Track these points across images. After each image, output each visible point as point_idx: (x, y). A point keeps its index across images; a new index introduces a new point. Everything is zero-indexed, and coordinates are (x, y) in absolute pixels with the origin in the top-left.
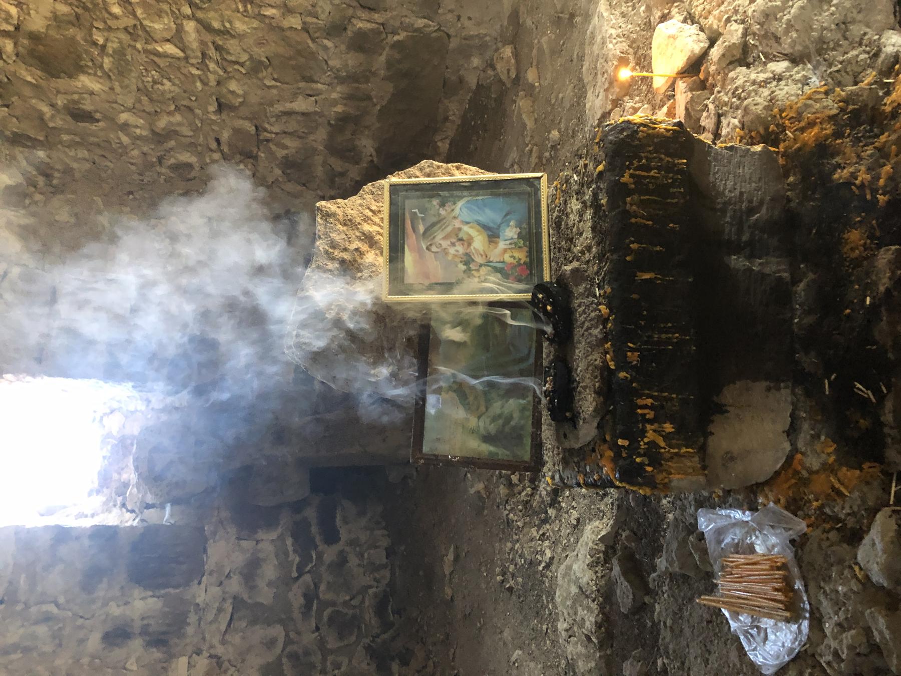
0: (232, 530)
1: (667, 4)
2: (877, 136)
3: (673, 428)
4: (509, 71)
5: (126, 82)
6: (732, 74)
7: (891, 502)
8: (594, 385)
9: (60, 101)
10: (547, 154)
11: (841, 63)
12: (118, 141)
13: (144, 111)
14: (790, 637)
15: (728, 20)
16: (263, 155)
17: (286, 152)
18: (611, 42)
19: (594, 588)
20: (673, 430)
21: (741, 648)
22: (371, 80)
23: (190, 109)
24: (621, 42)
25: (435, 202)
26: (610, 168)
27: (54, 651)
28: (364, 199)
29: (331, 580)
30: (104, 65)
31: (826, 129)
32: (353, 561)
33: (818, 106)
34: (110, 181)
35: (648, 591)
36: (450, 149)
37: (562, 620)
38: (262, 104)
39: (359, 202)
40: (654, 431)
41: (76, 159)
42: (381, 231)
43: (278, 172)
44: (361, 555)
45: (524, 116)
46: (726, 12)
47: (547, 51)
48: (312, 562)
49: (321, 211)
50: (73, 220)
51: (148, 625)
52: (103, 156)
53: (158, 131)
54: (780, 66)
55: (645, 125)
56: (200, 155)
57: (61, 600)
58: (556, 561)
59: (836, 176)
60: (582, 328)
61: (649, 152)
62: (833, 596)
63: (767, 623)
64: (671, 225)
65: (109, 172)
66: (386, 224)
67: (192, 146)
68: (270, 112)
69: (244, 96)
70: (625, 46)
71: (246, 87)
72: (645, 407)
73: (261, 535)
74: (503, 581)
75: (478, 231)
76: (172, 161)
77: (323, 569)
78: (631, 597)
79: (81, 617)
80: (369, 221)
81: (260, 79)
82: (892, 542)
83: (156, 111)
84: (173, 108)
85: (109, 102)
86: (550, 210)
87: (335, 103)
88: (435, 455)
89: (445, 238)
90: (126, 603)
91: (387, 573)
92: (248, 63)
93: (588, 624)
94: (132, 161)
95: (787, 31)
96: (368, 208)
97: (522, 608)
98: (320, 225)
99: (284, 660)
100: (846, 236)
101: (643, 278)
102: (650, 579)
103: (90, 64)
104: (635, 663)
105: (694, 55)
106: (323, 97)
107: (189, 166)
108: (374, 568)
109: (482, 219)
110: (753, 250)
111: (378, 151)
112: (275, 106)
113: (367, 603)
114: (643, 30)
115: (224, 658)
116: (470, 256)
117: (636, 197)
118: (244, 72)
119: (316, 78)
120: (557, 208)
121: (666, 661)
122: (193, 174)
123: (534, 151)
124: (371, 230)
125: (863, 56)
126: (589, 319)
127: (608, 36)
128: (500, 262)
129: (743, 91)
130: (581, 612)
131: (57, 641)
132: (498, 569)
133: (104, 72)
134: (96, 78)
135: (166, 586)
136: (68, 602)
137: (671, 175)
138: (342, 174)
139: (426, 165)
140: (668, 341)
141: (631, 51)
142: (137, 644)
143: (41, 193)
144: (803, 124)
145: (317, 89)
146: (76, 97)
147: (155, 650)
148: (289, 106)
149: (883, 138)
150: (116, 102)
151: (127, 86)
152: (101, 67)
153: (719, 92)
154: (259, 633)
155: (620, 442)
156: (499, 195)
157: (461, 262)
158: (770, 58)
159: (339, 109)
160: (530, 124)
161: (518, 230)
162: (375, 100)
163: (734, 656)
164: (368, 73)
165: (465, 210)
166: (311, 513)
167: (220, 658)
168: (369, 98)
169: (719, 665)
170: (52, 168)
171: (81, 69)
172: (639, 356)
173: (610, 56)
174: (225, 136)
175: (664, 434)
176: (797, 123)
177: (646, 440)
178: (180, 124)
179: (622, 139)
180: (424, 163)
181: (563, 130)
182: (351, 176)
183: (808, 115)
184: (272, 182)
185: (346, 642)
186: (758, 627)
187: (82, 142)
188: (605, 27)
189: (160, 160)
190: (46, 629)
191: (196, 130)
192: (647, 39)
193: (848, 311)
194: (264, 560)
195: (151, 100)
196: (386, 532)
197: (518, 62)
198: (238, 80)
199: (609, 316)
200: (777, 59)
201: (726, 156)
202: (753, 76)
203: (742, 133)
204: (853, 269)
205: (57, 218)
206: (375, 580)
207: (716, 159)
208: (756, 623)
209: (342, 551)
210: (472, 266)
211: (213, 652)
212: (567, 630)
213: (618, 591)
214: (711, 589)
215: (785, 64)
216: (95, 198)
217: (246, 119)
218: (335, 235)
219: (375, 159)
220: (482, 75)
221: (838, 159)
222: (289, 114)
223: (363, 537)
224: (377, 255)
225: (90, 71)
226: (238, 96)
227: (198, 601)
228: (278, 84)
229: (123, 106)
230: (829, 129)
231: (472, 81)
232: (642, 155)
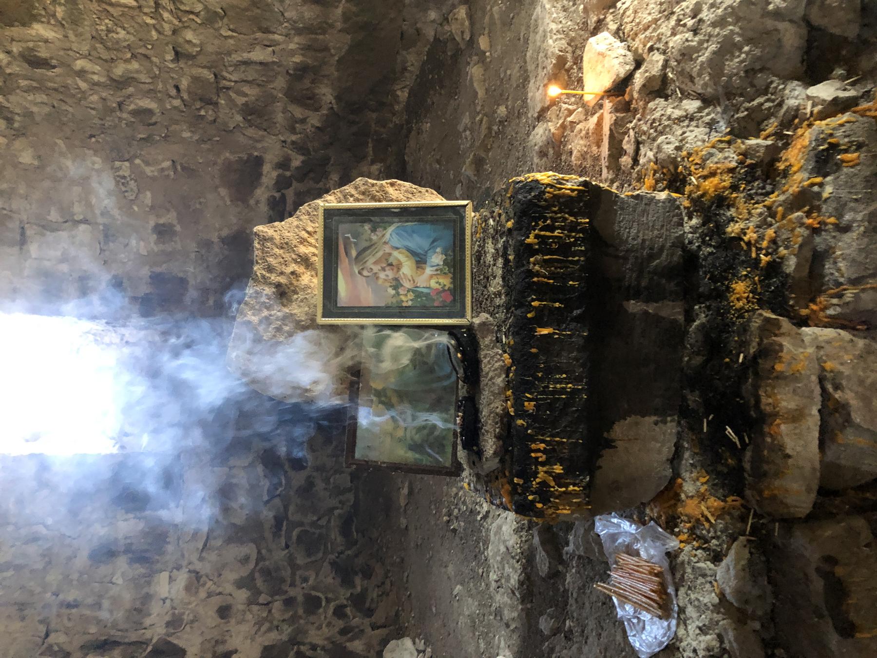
1: (603, 9)
2: (767, 194)
3: (562, 469)
4: (463, 32)
5: (80, 30)
6: (651, 105)
7: (747, 533)
8: (495, 431)
9: (15, 48)
10: (495, 128)
11: (747, 109)
12: (76, 87)
13: (100, 58)
14: (662, 631)
15: (651, 49)
16: (223, 102)
18: (551, 38)
19: (519, 551)
20: (562, 471)
21: (624, 631)
22: (329, 31)
23: (146, 57)
24: (561, 39)
25: (367, 227)
26: (518, 227)
28: (301, 220)
30: (57, 14)
31: (725, 181)
32: (320, 485)
33: (720, 155)
34: (71, 124)
35: (561, 561)
36: (409, 96)
37: (493, 571)
38: (221, 53)
39: (296, 223)
40: (546, 472)
42: (316, 252)
43: (239, 118)
45: (475, 85)
46: (650, 38)
47: (498, 22)
49: (259, 236)
50: (36, 163)
51: (131, 544)
53: (114, 77)
54: (692, 105)
55: (552, 186)
56: (160, 101)
58: (491, 515)
59: (729, 229)
60: (487, 377)
61: (555, 212)
62: (696, 603)
63: (646, 616)
64: (571, 283)
65: (70, 116)
66: (320, 245)
67: (151, 93)
68: (228, 61)
69: (201, 45)
70: (563, 43)
71: (201, 37)
72: (539, 450)
74: (448, 521)
75: (407, 257)
78: (547, 565)
80: (305, 243)
81: (215, 29)
82: (744, 570)
83: (112, 59)
84: (129, 55)
85: (65, 49)
86: (473, 243)
87: (292, 53)
88: (365, 461)
89: (375, 263)
91: (351, 497)
92: (202, 13)
93: (512, 581)
94: (92, 106)
95: (700, 74)
96: (305, 230)
97: (463, 549)
98: (258, 250)
99: (257, 575)
100: (733, 286)
101: (542, 333)
102: (564, 552)
103: (43, 13)
104: (549, 619)
105: (620, 78)
106: (281, 47)
107: (150, 112)
109: (412, 245)
110: (653, 294)
111: (338, 98)
112: (233, 56)
114: (581, 29)
115: (202, 573)
116: (398, 281)
117: (539, 257)
118: (199, 21)
119: (272, 29)
120: (478, 243)
121: (571, 624)
123: (484, 122)
124: (307, 251)
125: (767, 105)
126: (493, 369)
127: (549, 30)
128: (427, 288)
129: (659, 125)
130: (508, 570)
132: (444, 510)
133: (57, 20)
134: (50, 26)
137: (574, 234)
138: (303, 121)
139: (362, 183)
140: (563, 391)
141: (570, 49)
142: (122, 563)
144: (705, 172)
145: (275, 41)
146: (31, 44)
148: (246, 56)
149: (773, 197)
150: (71, 49)
151: (81, 34)
152: (54, 15)
153: (639, 120)
155: (516, 480)
156: (427, 222)
157: (391, 286)
158: (686, 95)
159: (297, 59)
160: (481, 93)
161: (444, 257)
162: (333, 51)
163: (619, 638)
164: (325, 25)
165: (394, 235)
167: (198, 573)
168: (326, 49)
169: (609, 641)
170: (12, 112)
171: (35, 18)
172: (535, 406)
173: (549, 53)
174: (184, 83)
175: (554, 474)
176: (701, 170)
177: (538, 480)
178: (137, 72)
179: (530, 200)
180: (359, 181)
181: (510, 107)
182: (312, 122)
183: (711, 164)
184: (234, 128)
185: (313, 559)
186: (638, 618)
187: (41, 88)
188: (547, 21)
191: (155, 77)
192: (584, 40)
193: (727, 360)
195: (107, 48)
197: (472, 24)
198: (194, 30)
199: (512, 366)
200: (691, 97)
201: (632, 204)
202: (669, 111)
203: (655, 167)
204: (737, 318)
205: (21, 160)
206: (340, 502)
207: (622, 209)
208: (637, 614)
210: (401, 291)
211: (191, 567)
212: (496, 581)
213: (538, 557)
214: (605, 577)
215: (697, 104)
216: (57, 141)
217: (204, 67)
218: (271, 260)
219: (335, 106)
220: (439, 29)
221: (732, 212)
222: (247, 63)
224: (312, 276)
225: (43, 19)
226: (195, 45)
228: (235, 34)
229: (78, 53)
230: (727, 180)
231: (430, 33)
232: (548, 215)
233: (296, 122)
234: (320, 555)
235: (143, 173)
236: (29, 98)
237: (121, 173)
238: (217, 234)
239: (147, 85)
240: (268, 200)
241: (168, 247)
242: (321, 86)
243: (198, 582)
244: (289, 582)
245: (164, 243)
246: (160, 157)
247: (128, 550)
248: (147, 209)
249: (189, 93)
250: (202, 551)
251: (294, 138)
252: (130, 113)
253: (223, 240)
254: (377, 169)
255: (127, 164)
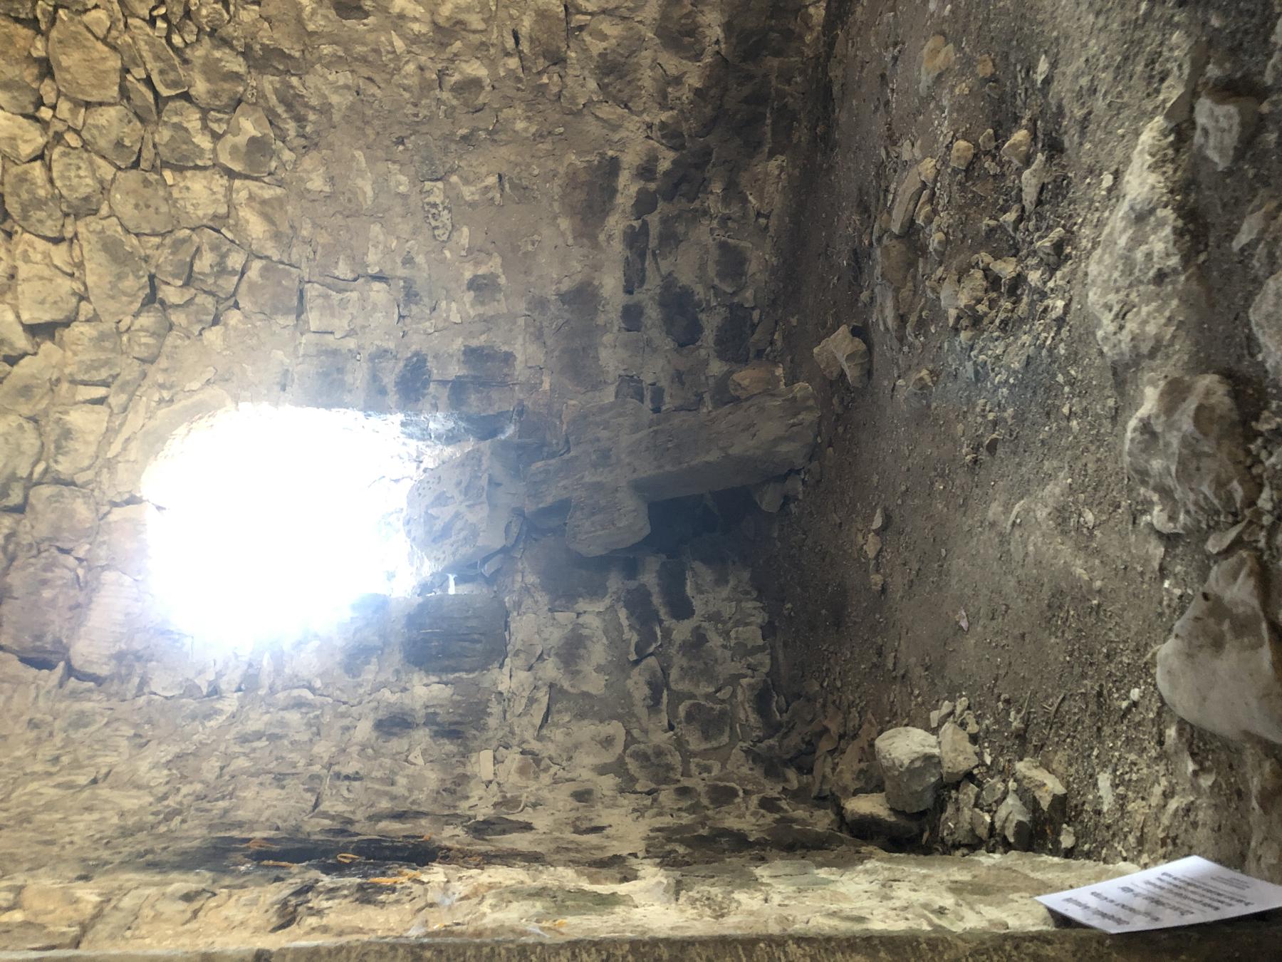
0: (543, 599)
12: (389, 48)
16: (573, 55)
17: (604, 44)
27: (311, 740)
29: (685, 665)
32: (715, 641)
41: (337, 89)
44: (726, 634)
48: (656, 640)
50: (327, 189)
51: (435, 714)
52: (370, 79)
56: (492, 64)
57: (318, 684)
65: (376, 104)
73: (582, 605)
76: (457, 77)
77: (673, 651)
79: (344, 703)
90: (404, 690)
99: (627, 760)
108: (742, 650)
111: (728, 27)
113: (740, 697)
122: (482, 99)
131: (314, 729)
135: (454, 670)
136: (326, 686)
138: (678, 81)
143: (291, 150)
147: (446, 741)
154: (588, 730)
166: (649, 578)
182: (691, 81)
184: (584, 105)
185: (714, 744)
189: (442, 74)
190: (299, 716)
194: (588, 638)
196: (758, 604)
205: (309, 185)
209: (699, 627)
223: (728, 610)
227: (501, 688)
233: (669, 84)
234: (725, 739)
235: (459, 196)
236: (331, 78)
237: (431, 199)
238: (554, 288)
239: (477, 36)
240: (625, 233)
241: (489, 310)
242: (706, 9)
243: (538, 766)
244: (680, 769)
245: (482, 303)
246: (484, 170)
247: (430, 720)
248: (464, 253)
249: (532, 40)
250: (541, 727)
251: (665, 116)
252: (452, 89)
253: (563, 298)
254: (778, 167)
255: (440, 184)
